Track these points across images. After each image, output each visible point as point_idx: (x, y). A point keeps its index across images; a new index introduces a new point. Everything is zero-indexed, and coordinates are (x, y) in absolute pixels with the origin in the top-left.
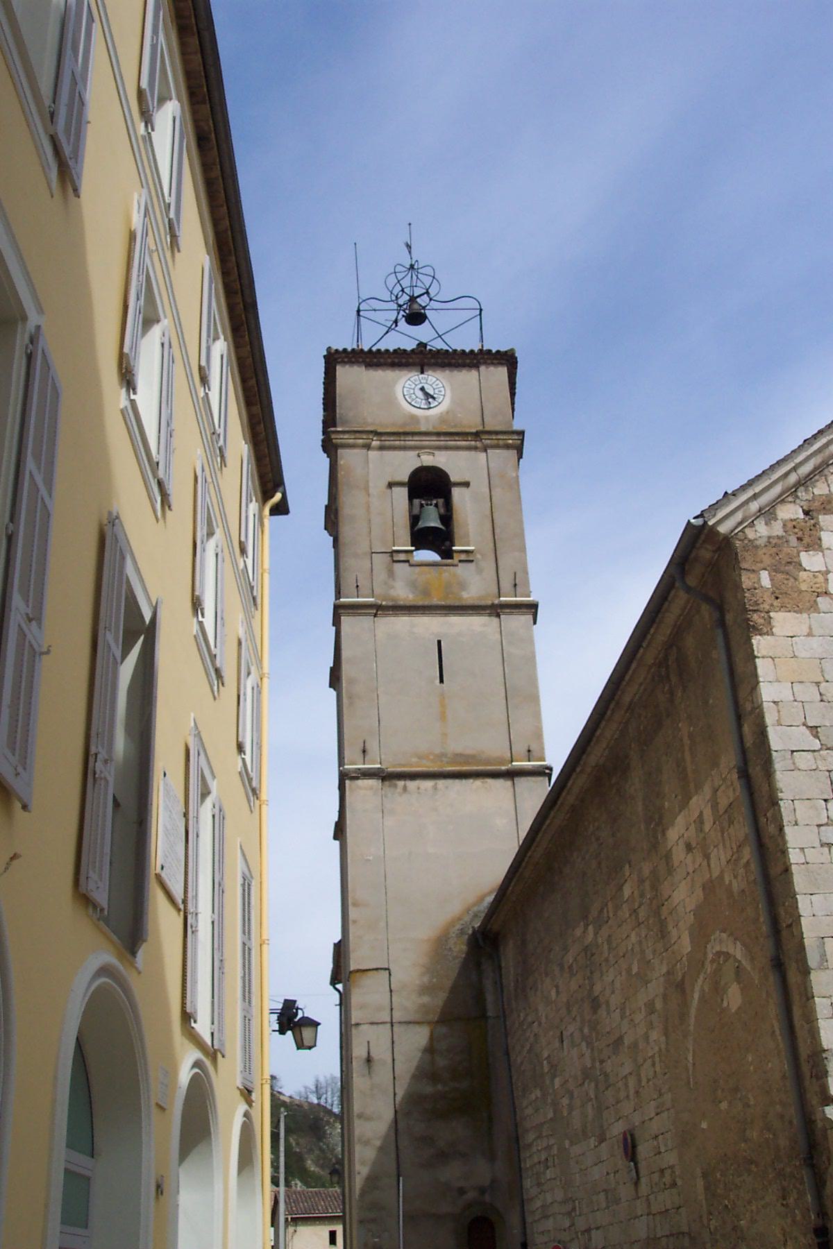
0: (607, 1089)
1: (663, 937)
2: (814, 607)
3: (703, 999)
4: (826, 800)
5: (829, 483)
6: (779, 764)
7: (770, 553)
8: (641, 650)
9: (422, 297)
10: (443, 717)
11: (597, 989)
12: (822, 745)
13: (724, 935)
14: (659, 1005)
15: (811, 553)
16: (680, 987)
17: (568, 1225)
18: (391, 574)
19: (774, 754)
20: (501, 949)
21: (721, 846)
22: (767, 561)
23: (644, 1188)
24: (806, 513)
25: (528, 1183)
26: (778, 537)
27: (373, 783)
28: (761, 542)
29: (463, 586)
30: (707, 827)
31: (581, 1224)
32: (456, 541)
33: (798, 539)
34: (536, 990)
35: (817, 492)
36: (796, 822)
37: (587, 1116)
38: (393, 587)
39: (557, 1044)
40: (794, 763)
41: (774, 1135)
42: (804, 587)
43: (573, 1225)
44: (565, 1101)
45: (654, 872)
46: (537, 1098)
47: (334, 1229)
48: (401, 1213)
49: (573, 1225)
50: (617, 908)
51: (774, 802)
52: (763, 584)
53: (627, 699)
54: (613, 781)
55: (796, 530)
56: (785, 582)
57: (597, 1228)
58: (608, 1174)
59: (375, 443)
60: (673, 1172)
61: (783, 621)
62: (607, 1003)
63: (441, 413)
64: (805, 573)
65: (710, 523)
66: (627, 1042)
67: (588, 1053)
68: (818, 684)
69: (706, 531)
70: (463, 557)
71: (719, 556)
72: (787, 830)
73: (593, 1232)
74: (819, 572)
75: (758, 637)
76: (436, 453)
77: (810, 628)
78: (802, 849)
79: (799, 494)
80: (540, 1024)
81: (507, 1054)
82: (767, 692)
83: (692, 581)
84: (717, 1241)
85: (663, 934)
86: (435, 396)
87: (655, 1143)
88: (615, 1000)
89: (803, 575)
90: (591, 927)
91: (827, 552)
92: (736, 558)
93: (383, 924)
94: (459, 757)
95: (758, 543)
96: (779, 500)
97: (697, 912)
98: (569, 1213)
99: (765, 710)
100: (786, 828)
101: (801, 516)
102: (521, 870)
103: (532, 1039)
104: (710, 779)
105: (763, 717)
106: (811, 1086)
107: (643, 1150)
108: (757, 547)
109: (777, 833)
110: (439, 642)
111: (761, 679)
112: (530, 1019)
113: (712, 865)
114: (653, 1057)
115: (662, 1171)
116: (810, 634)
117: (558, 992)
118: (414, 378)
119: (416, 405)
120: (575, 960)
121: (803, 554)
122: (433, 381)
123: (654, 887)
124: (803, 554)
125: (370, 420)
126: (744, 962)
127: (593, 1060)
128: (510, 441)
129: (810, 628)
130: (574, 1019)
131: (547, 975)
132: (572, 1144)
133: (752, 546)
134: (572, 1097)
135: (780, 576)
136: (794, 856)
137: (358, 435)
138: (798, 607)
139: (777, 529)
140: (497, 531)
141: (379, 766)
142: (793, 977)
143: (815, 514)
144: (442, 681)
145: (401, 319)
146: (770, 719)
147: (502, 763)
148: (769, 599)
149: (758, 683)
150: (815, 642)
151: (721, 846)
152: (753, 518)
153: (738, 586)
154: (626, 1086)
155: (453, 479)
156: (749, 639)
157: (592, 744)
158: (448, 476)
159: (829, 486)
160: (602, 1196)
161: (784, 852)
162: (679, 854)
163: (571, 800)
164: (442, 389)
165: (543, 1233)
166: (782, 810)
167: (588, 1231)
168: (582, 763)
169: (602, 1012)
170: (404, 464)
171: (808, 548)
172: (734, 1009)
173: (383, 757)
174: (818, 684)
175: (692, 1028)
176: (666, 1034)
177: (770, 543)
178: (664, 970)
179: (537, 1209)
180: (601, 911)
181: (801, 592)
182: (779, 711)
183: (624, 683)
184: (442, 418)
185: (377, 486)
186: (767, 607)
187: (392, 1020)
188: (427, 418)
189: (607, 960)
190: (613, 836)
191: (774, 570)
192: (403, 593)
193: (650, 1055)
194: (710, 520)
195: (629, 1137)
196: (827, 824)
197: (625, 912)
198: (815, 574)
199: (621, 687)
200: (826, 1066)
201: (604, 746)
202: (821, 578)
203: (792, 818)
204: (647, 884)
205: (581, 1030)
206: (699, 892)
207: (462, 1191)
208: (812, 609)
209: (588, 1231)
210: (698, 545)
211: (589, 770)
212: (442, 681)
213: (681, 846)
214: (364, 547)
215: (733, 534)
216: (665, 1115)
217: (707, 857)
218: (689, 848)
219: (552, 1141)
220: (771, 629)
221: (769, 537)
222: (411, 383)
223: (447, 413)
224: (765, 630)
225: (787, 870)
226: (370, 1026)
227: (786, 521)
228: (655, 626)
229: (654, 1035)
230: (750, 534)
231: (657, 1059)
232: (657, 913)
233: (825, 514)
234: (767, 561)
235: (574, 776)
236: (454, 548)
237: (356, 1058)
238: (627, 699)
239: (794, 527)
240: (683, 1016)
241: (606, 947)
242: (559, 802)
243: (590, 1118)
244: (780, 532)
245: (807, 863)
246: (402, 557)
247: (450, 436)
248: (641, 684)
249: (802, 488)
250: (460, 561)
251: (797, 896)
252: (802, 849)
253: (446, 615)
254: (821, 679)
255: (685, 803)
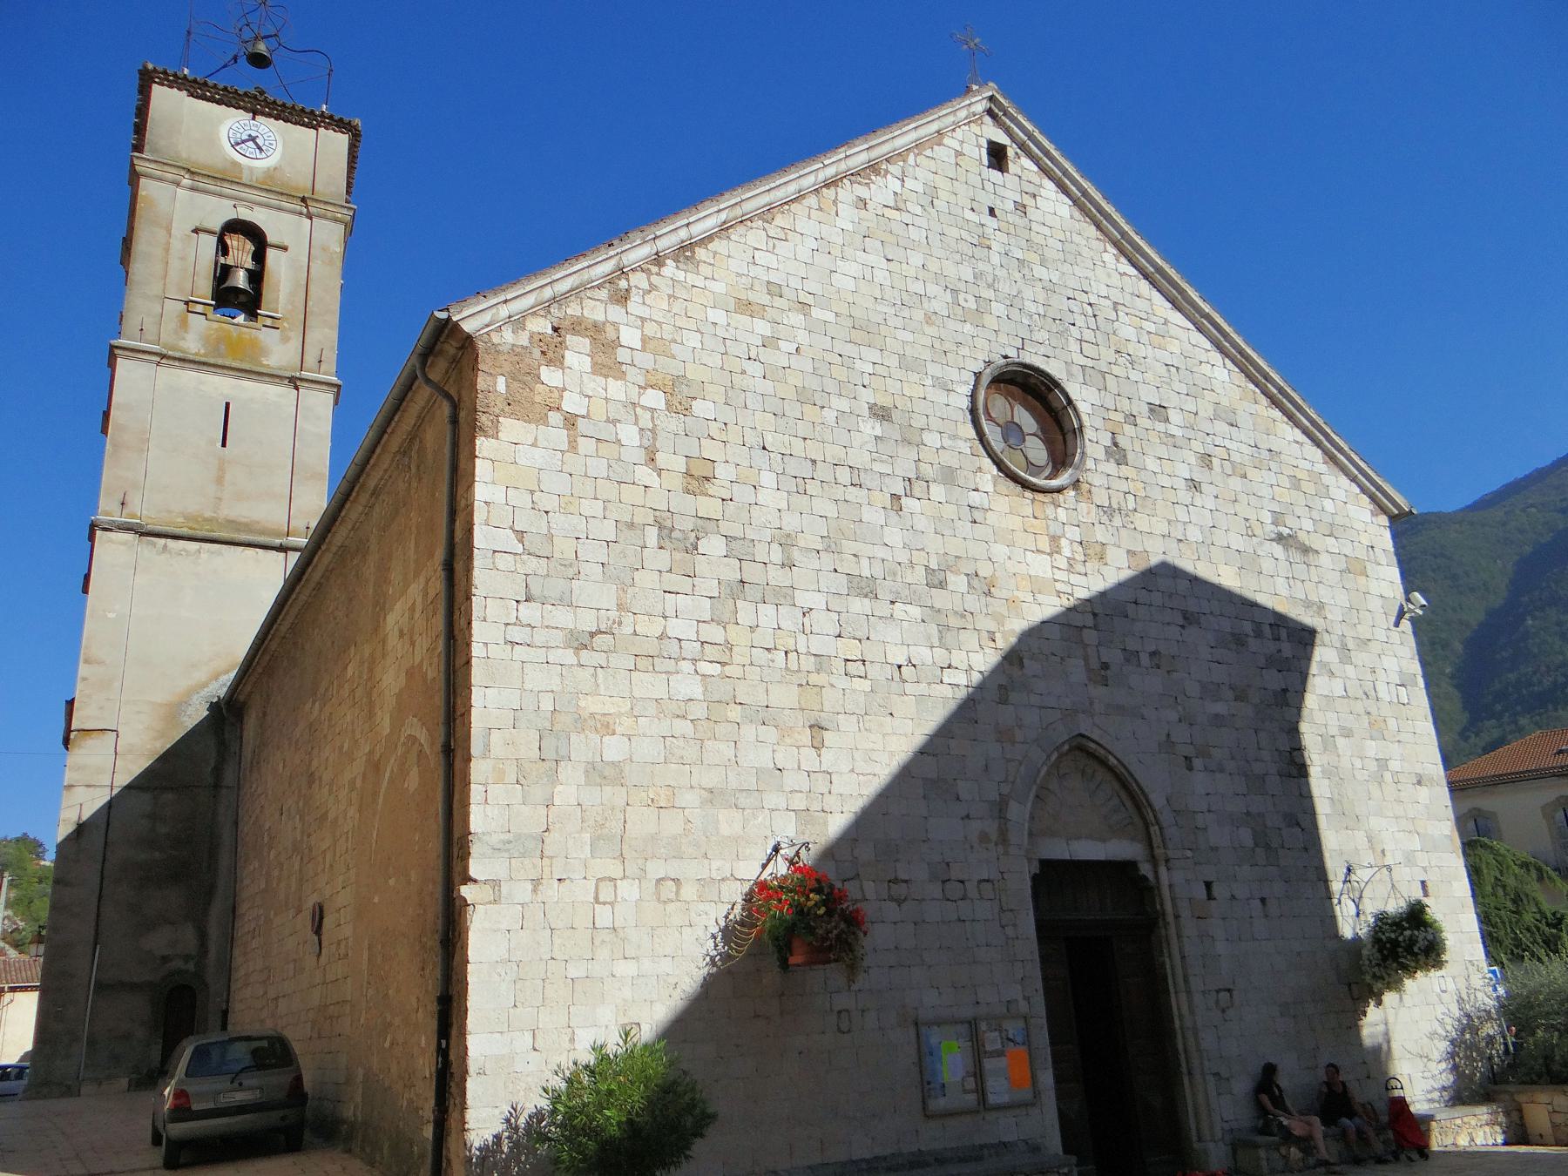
0: (309, 862)
1: (370, 718)
2: (544, 420)
3: (391, 781)
4: (517, 601)
5: (584, 305)
6: (478, 562)
7: (511, 360)
8: (386, 436)
9: (270, 39)
10: (220, 480)
11: (315, 763)
12: (524, 549)
13: (415, 720)
14: (359, 783)
15: (551, 368)
16: (375, 767)
17: (262, 993)
18: (184, 324)
19: (475, 550)
20: (246, 718)
21: (424, 635)
22: (507, 367)
23: (323, 959)
24: (555, 329)
25: (236, 952)
26: (522, 347)
27: (129, 537)
28: (505, 348)
29: (264, 352)
30: (417, 615)
31: (272, 994)
32: (263, 304)
33: (542, 352)
34: (268, 763)
35: (569, 311)
36: (484, 618)
37: (290, 888)
38: (184, 339)
39: (277, 815)
40: (493, 563)
41: (424, 910)
42: (538, 399)
43: (266, 993)
44: (276, 873)
45: (372, 655)
46: (255, 869)
47: (1450, 938)
48: (93, 980)
49: (266, 993)
50: (340, 686)
51: (468, 598)
52: (498, 389)
53: (372, 484)
54: (355, 562)
55: (541, 344)
56: (521, 391)
57: (284, 996)
58: (298, 944)
59: (186, 182)
60: (347, 943)
61: (511, 428)
62: (320, 778)
63: (268, 169)
64: (541, 386)
65: (455, 319)
66: (331, 816)
67: (299, 825)
68: (532, 492)
69: (449, 327)
70: (269, 322)
71: (462, 354)
72: (475, 624)
73: (280, 1000)
74: (556, 388)
75: (483, 438)
76: (256, 208)
77: (536, 439)
78: (486, 644)
79: (552, 310)
80: (266, 796)
81: (236, 823)
82: (482, 492)
83: (435, 374)
84: (370, 1008)
85: (371, 715)
86: (264, 148)
87: (337, 915)
88: (327, 777)
89: (539, 387)
90: (317, 704)
91: (567, 371)
92: (476, 359)
93: (117, 684)
94: (232, 524)
95: (501, 348)
96: (531, 311)
97: (399, 696)
98: (264, 982)
99: (475, 508)
100: (473, 622)
101: (550, 331)
102: (266, 642)
103: (258, 811)
104: (426, 569)
105: (472, 515)
106: (457, 869)
107: (328, 922)
108: (498, 352)
109: (465, 627)
110: (227, 405)
111: (477, 479)
112: (259, 791)
113: (416, 652)
114: (347, 833)
115: (339, 943)
116: (534, 445)
117: (284, 767)
118: (245, 122)
119: (251, 156)
120: (302, 735)
121: (543, 368)
122: (265, 131)
123: (371, 670)
124: (543, 368)
125: (184, 155)
126: (425, 747)
127: (303, 833)
128: (339, 215)
129: (536, 439)
130: (293, 793)
131: (278, 749)
132: (276, 914)
133: (495, 350)
134: (282, 870)
135: (516, 384)
136: (477, 650)
137: (166, 168)
138: (528, 416)
139: (523, 339)
140: (310, 303)
141: (138, 521)
142: (458, 764)
143: (562, 332)
144: (224, 445)
145: (242, 56)
146: (478, 517)
147: (278, 535)
148: (501, 404)
149: (474, 481)
150: (538, 452)
151: (424, 635)
152: (501, 323)
153: (473, 385)
154: (324, 858)
155: (270, 239)
156: (474, 438)
157: (337, 523)
158: (265, 236)
159: (582, 309)
160: (292, 966)
161: (469, 645)
162: (393, 641)
163: (317, 576)
164: (274, 142)
165: (241, 1001)
166: (473, 605)
167: (276, 999)
168: (327, 541)
169: (316, 786)
170: (219, 212)
171: (550, 363)
172: (412, 789)
173: (144, 512)
174: (532, 492)
175: (379, 807)
176: (360, 811)
177: (513, 350)
178: (367, 750)
179: (241, 978)
180: (327, 690)
181: (533, 403)
182: (489, 512)
183: (368, 466)
184: (270, 174)
185: (181, 227)
186: (497, 411)
187: (112, 783)
188: (251, 169)
189: (325, 736)
190: (347, 616)
191: (512, 377)
192: (192, 345)
193: (345, 831)
194: (455, 315)
195: (317, 910)
196: (515, 624)
197: (345, 692)
198: (551, 389)
199: (367, 470)
200: (469, 848)
201: (350, 527)
202: (556, 394)
203: (481, 614)
204: (366, 665)
205: (297, 803)
206: (403, 679)
207: (165, 959)
208: (541, 421)
209: (276, 999)
210: (442, 339)
211: (334, 549)
212: (224, 445)
213: (396, 633)
214: (155, 289)
215: (477, 334)
216: (348, 889)
217: (413, 644)
218: (401, 634)
219: (261, 911)
220: (497, 433)
221: (513, 345)
222: (240, 127)
223: (275, 169)
224: (491, 433)
225: (468, 663)
226: (86, 788)
227: (533, 333)
228: (399, 413)
229: (352, 812)
230: (495, 338)
231: (350, 835)
232: (369, 695)
233: (572, 334)
234: (507, 367)
235: (320, 553)
236: (259, 311)
237: (64, 820)
238: (372, 484)
239: (541, 341)
240: (375, 794)
241: (327, 722)
242: (305, 578)
243: (293, 889)
244: (526, 343)
245: (488, 658)
246: (199, 308)
247: (273, 189)
248: (386, 471)
249: (556, 305)
250: (264, 326)
251: (472, 688)
252: (486, 644)
253: (239, 378)
254: (537, 488)
255: (404, 592)
